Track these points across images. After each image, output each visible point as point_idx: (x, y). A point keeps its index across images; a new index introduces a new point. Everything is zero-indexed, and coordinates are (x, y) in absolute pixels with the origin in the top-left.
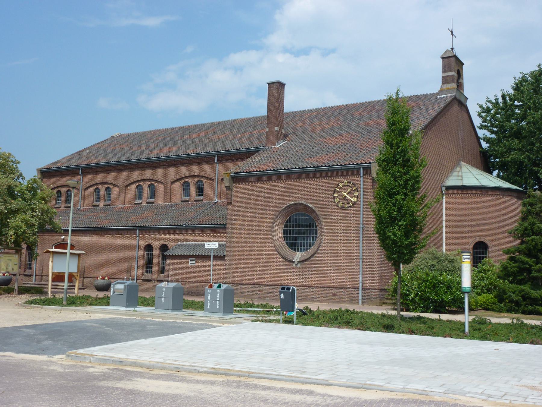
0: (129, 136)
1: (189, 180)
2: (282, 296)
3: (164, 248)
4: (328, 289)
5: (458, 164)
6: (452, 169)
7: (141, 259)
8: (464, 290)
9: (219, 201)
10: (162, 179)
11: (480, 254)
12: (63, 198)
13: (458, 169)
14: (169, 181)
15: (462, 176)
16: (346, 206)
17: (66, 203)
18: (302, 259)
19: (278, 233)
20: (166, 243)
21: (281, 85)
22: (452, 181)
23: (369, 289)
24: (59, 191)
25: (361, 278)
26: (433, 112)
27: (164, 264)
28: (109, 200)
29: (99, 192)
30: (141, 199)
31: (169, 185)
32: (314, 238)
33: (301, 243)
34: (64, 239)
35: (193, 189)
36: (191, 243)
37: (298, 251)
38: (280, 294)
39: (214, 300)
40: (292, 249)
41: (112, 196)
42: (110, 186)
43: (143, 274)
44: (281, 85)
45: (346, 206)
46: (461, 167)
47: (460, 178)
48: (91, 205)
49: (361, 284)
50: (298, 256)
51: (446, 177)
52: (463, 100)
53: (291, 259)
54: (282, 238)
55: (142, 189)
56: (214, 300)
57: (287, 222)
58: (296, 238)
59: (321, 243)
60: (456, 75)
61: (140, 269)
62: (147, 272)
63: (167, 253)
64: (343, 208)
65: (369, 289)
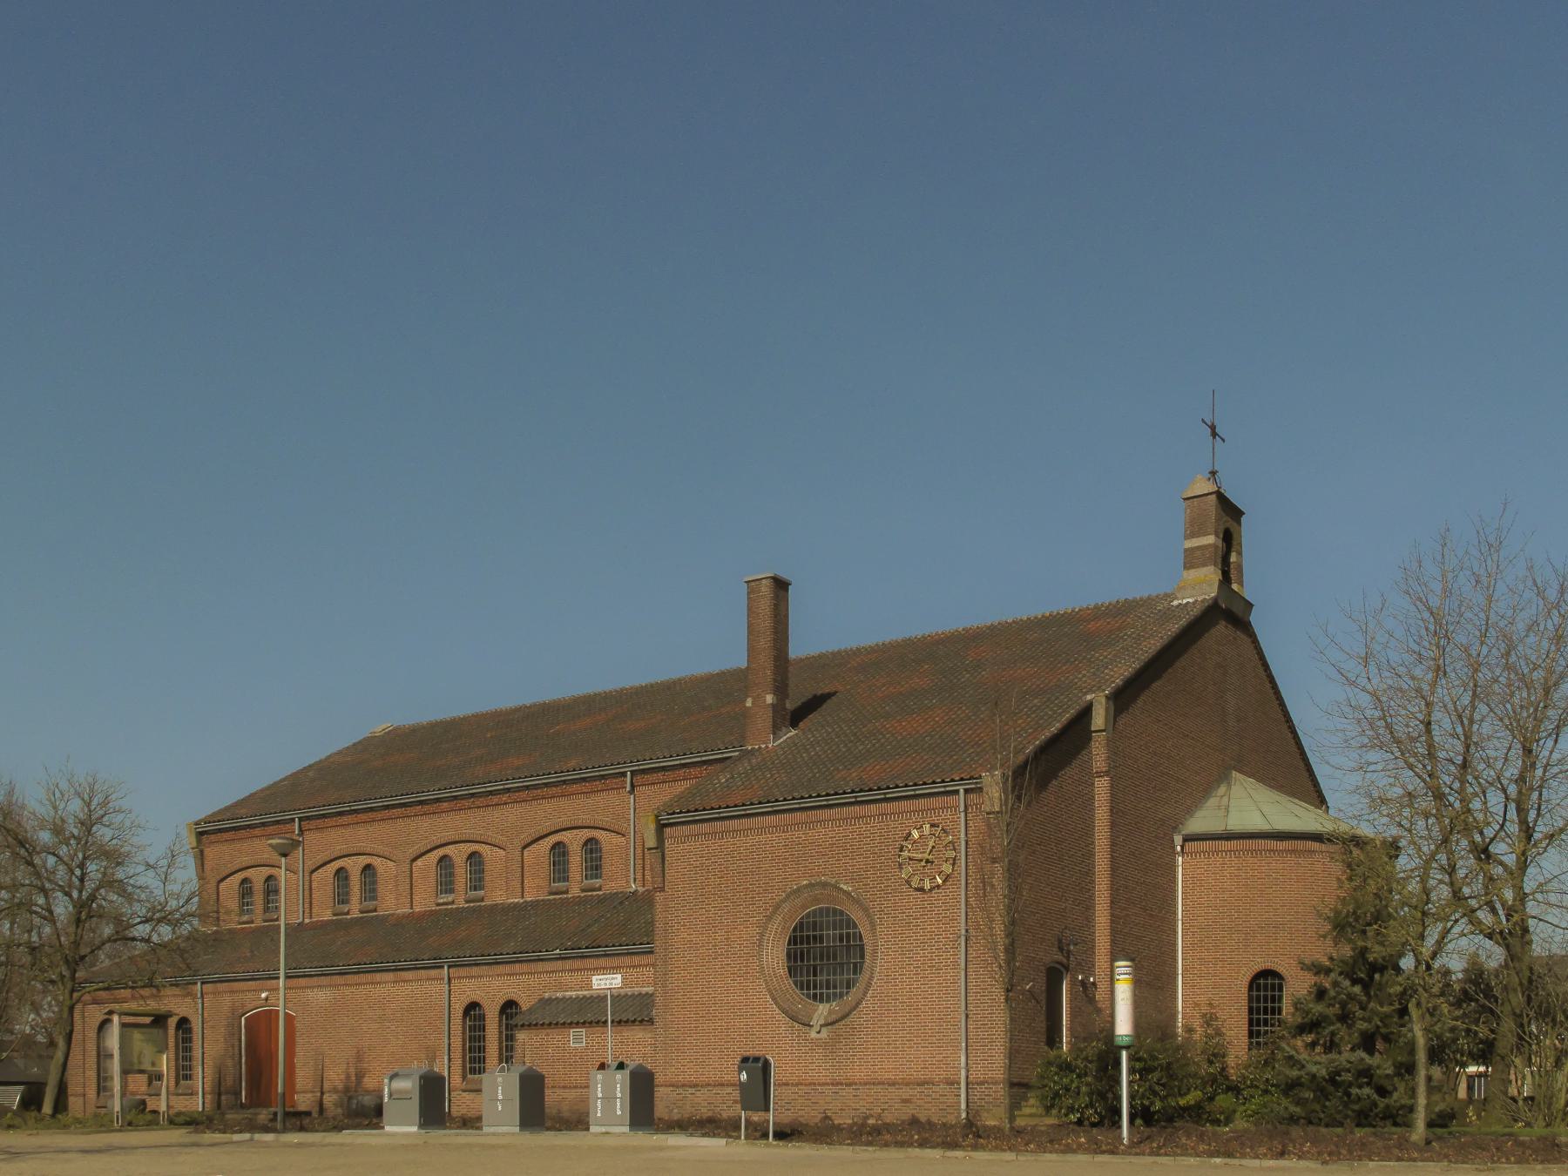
0: (414, 731)
1: (564, 837)
2: (744, 1076)
3: (509, 1007)
4: (891, 1089)
5: (1223, 777)
6: (1207, 791)
7: (457, 1042)
8: (1119, 1042)
9: (641, 889)
10: (499, 839)
11: (1266, 1001)
12: (258, 898)
13: (1222, 789)
14: (518, 843)
15: (1227, 810)
16: (927, 886)
17: (266, 910)
18: (834, 1017)
19: (775, 956)
20: (514, 997)
21: (781, 585)
22: (1200, 822)
23: (982, 1083)
24: (245, 881)
25: (963, 1059)
26: (1153, 645)
27: (510, 1038)
28: (374, 898)
29: (347, 878)
30: (452, 891)
31: (518, 853)
32: (857, 968)
33: (828, 981)
34: (266, 999)
35: (576, 861)
36: (573, 994)
37: (821, 1001)
38: (740, 1072)
39: (609, 1099)
40: (808, 996)
41: (381, 888)
42: (376, 861)
43: (464, 1077)
44: (781, 585)
45: (927, 886)
46: (1229, 785)
47: (1222, 813)
48: (329, 912)
49: (963, 1072)
50: (822, 1011)
51: (1189, 812)
52: (1237, 609)
53: (805, 1020)
54: (782, 971)
55: (452, 866)
56: (609, 1099)
57: (795, 930)
58: (815, 968)
59: (871, 978)
60: (1220, 543)
61: (457, 1063)
62: (473, 1071)
63: (518, 1020)
64: (921, 890)
65: (982, 1083)
